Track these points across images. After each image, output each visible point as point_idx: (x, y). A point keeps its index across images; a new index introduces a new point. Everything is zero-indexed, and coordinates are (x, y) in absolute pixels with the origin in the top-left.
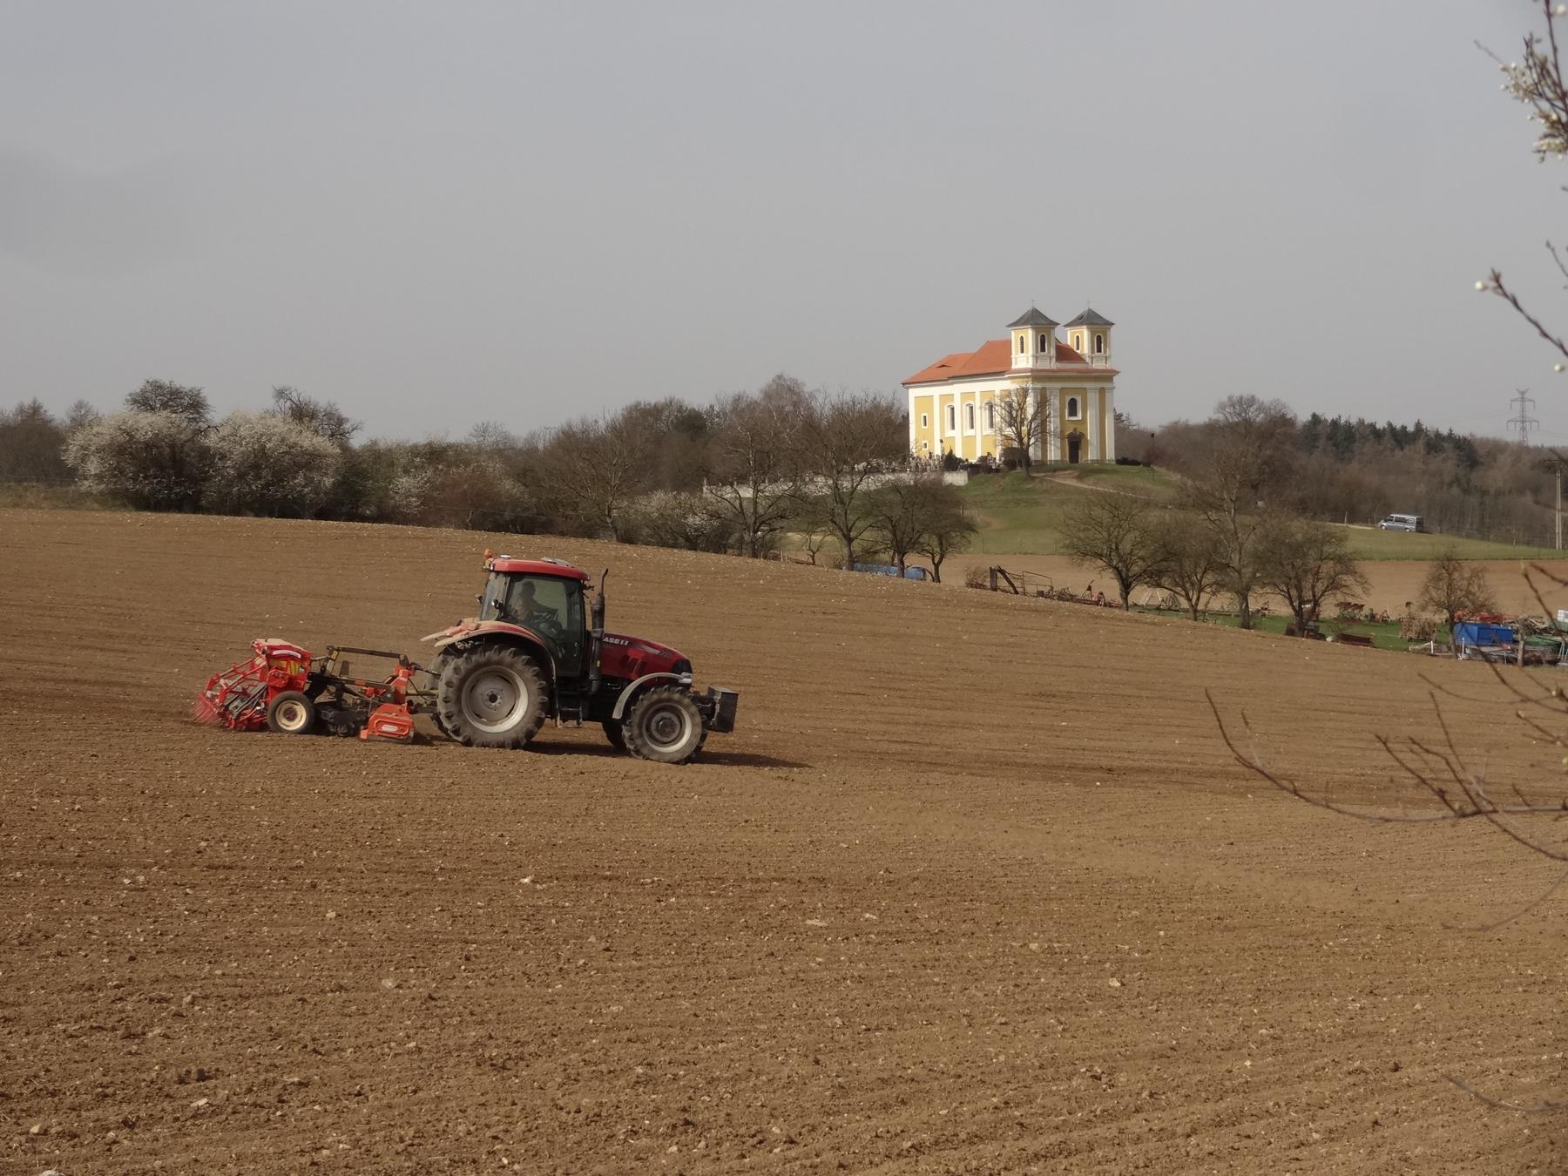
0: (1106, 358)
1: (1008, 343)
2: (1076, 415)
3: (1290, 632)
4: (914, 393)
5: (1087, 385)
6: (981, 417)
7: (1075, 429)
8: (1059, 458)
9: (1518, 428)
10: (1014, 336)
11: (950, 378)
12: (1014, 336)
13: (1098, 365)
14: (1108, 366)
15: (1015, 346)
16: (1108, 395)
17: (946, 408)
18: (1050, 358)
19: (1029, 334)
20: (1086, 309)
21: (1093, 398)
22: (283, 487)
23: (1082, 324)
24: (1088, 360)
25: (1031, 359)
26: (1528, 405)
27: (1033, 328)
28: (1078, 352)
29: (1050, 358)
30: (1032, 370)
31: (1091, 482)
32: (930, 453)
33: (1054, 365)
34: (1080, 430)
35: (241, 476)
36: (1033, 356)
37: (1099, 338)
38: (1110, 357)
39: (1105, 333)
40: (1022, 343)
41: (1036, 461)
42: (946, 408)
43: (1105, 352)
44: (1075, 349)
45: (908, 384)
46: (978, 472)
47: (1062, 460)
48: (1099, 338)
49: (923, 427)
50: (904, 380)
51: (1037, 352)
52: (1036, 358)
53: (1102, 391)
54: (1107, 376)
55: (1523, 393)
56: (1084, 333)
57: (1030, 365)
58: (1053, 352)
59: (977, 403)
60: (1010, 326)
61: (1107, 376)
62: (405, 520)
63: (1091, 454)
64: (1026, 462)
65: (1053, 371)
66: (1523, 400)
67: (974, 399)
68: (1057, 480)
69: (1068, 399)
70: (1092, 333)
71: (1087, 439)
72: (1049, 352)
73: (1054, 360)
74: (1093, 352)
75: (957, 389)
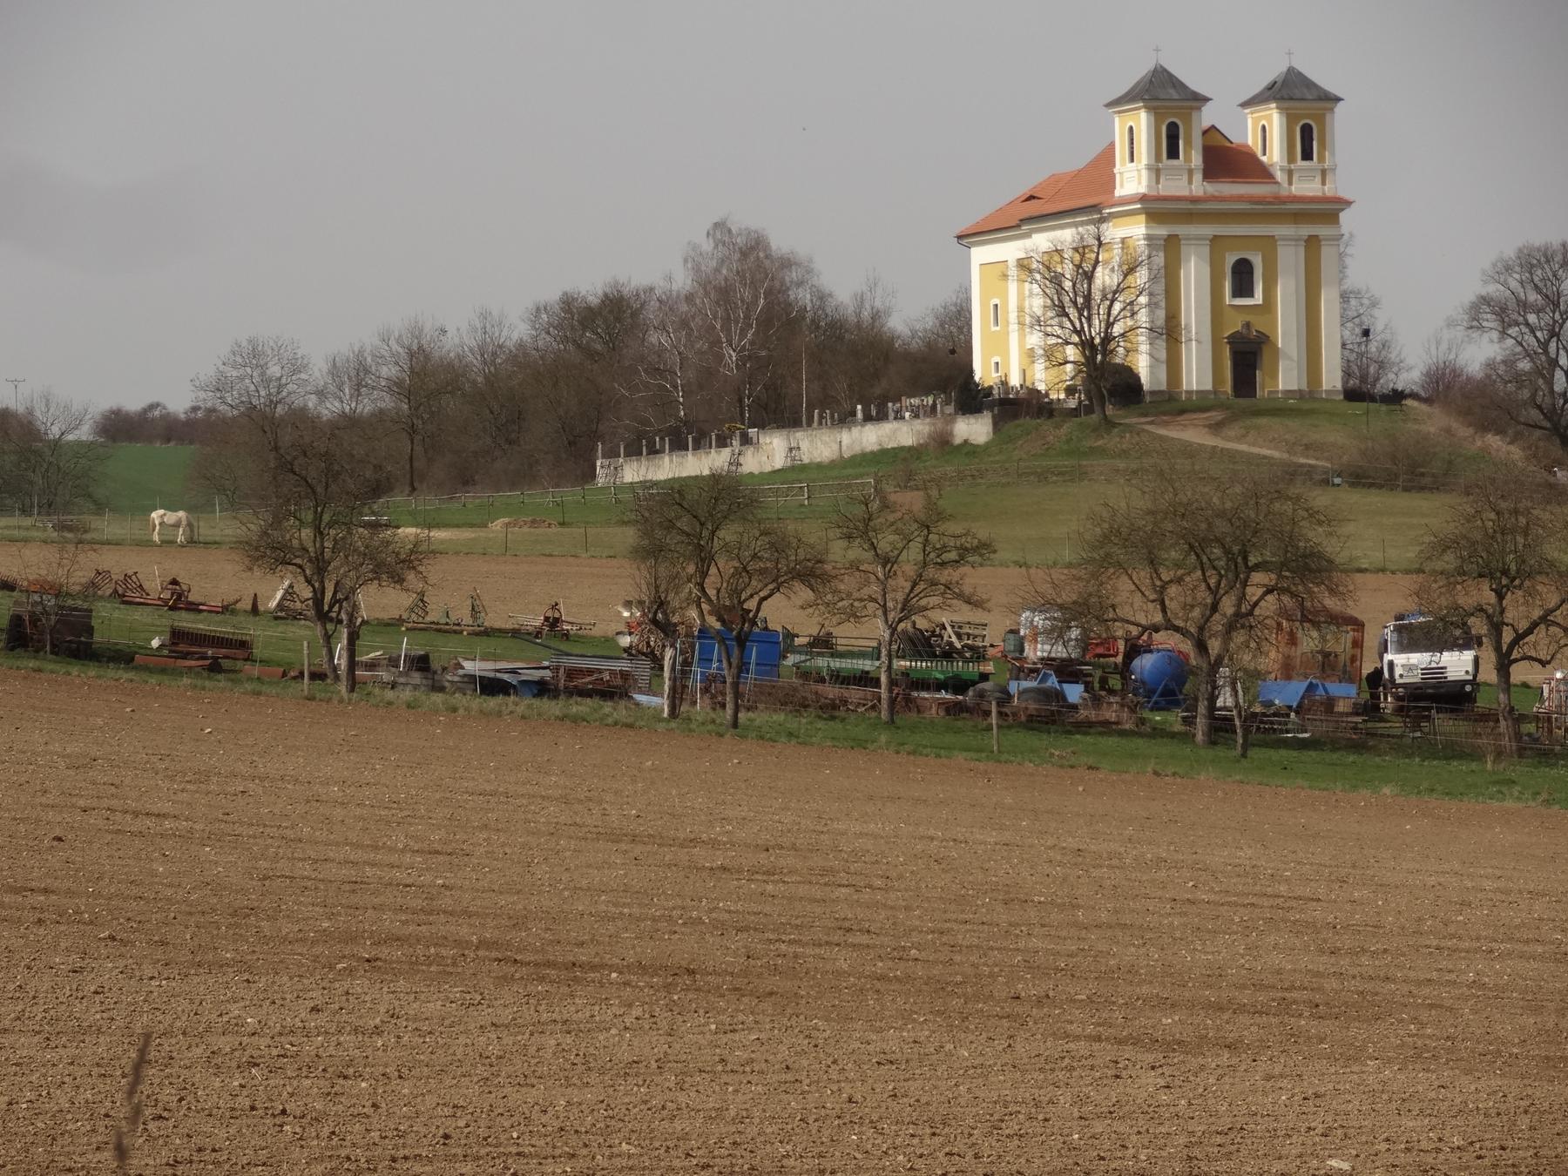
0: (1324, 173)
2: (1250, 294)
3: (172, 608)
4: (981, 255)
7: (1248, 325)
8: (1209, 386)
12: (1120, 125)
13: (1306, 186)
14: (1329, 190)
16: (1327, 253)
18: (1190, 172)
19: (1141, 120)
20: (1150, 66)
21: (1290, 259)
24: (1279, 176)
25: (1144, 173)
27: (1148, 109)
28: (1264, 159)
29: (1190, 172)
30: (1143, 199)
31: (1232, 433)
33: (1199, 187)
34: (1259, 324)
36: (1149, 168)
37: (1307, 132)
38: (1333, 170)
39: (1321, 120)
40: (1132, 148)
41: (1152, 393)
43: (1322, 159)
45: (967, 237)
46: (1016, 416)
47: (1215, 392)
50: (958, 232)
51: (1158, 158)
52: (1156, 172)
54: (1328, 211)
56: (1273, 118)
58: (1197, 159)
60: (1110, 105)
61: (1328, 211)
63: (1286, 377)
64: (1125, 388)
65: (1194, 200)
68: (1162, 432)
69: (1231, 259)
71: (1275, 346)
72: (1188, 159)
73: (1198, 177)
74: (1291, 159)
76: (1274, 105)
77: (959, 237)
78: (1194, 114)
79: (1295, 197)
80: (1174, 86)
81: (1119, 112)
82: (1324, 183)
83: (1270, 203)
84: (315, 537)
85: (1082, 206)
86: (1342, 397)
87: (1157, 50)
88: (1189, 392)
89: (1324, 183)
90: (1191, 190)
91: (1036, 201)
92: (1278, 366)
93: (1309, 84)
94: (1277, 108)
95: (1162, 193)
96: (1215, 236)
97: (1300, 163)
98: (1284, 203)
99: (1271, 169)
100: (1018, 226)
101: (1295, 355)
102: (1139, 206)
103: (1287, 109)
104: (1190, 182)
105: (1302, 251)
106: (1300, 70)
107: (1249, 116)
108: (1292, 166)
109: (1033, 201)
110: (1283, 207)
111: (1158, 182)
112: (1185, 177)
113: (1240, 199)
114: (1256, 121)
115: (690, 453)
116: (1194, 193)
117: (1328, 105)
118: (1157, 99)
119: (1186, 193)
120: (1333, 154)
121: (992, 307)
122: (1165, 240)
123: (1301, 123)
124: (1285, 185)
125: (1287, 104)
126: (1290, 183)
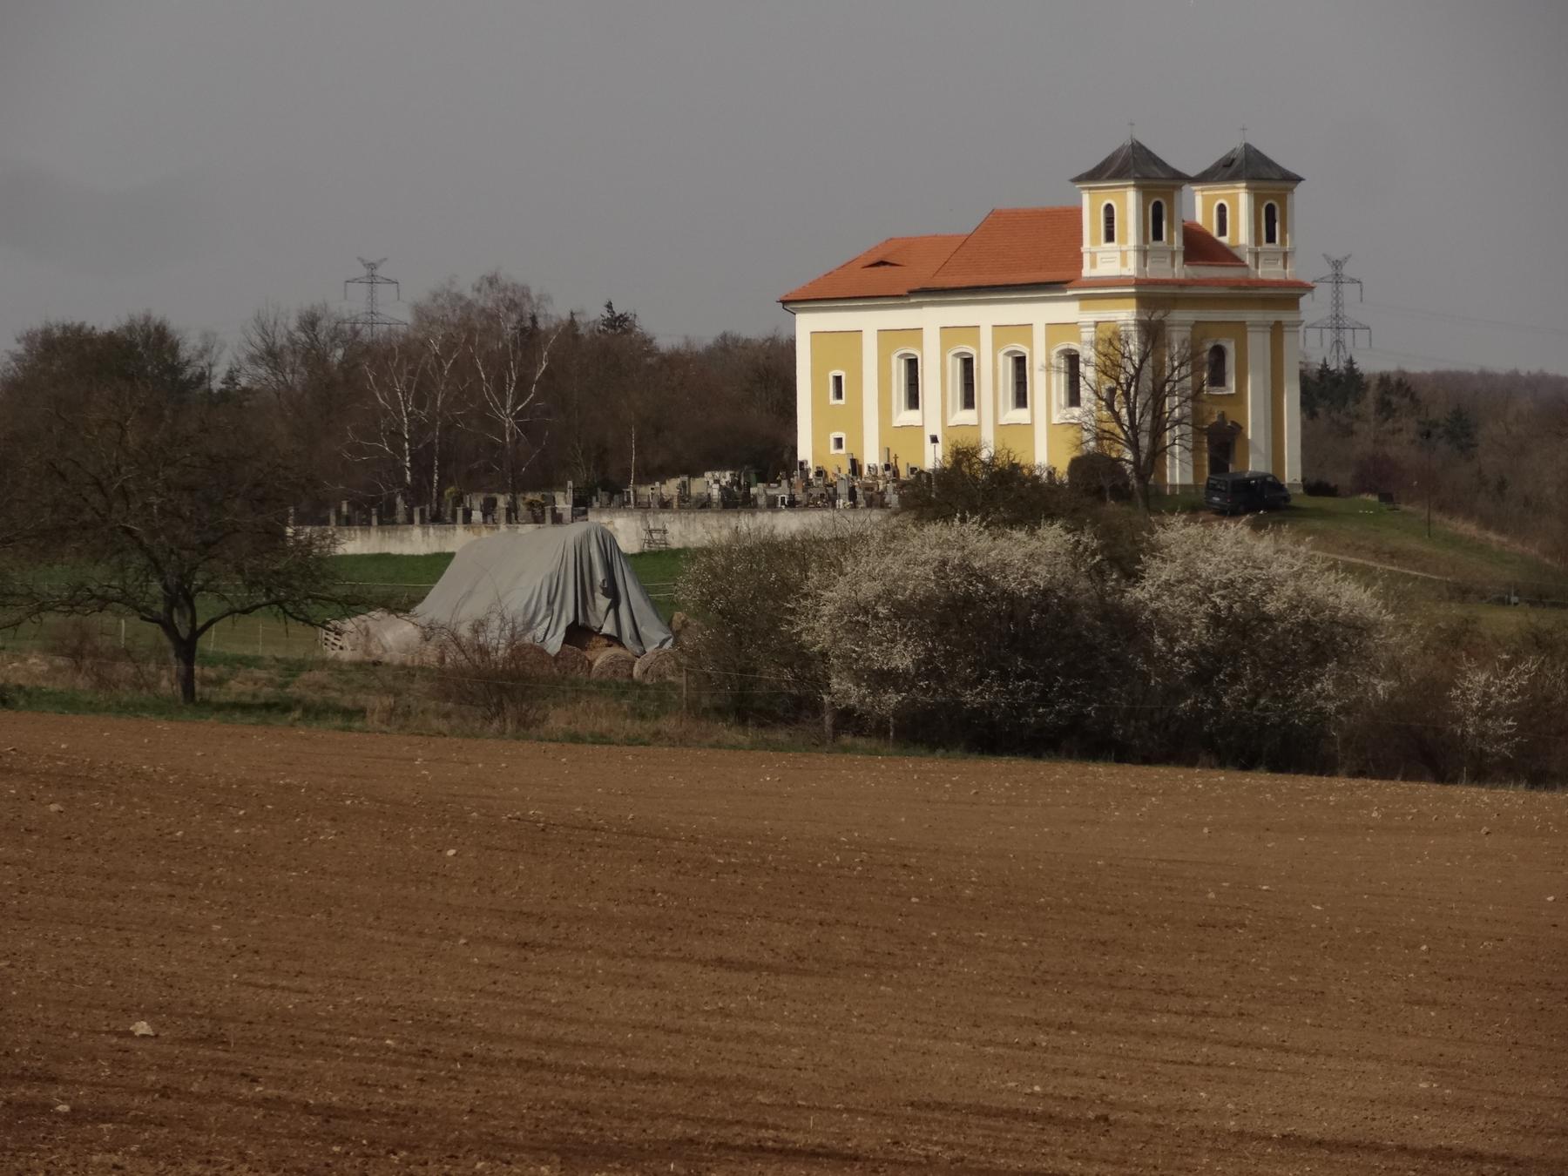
0: (1285, 254)
1: (1073, 217)
4: (807, 325)
5: (1251, 316)
6: (1046, 385)
7: (1222, 415)
8: (1190, 480)
9: (1327, 343)
10: (1090, 204)
11: (913, 293)
12: (1090, 204)
13: (1269, 271)
14: (1290, 273)
15: (1091, 224)
16: (1288, 338)
17: (894, 358)
18: (1173, 253)
19: (1128, 202)
21: (1258, 344)
22: (1287, 699)
23: (1234, 178)
24: (1248, 260)
25: (1132, 257)
26: (1349, 291)
27: (1138, 187)
28: (1225, 240)
29: (1173, 253)
30: (1138, 283)
32: (854, 462)
33: (1179, 270)
34: (1232, 416)
35: (1202, 678)
37: (1270, 210)
38: (1293, 252)
39: (1283, 199)
42: (894, 358)
44: (1214, 232)
45: (792, 303)
48: (1270, 210)
49: (833, 401)
50: (782, 295)
51: (1145, 241)
52: (1143, 253)
53: (1277, 330)
55: (1337, 264)
56: (1240, 200)
57: (1131, 269)
58: (1178, 242)
59: (1039, 357)
60: (1079, 179)
61: (1287, 296)
62: (1482, 773)
65: (1181, 284)
66: (1337, 280)
67: (977, 343)
70: (1257, 199)
71: (1245, 436)
72: (1170, 241)
73: (1179, 259)
74: (1258, 242)
75: (931, 319)
76: (1244, 185)
77: (785, 302)
78: (1176, 194)
79: (1263, 281)
80: (1156, 164)
81: (1090, 189)
82: (1285, 267)
83: (1245, 288)
84: (320, 604)
85: (1048, 280)
86: (1301, 491)
87: (1132, 124)
88: (1173, 486)
89: (1285, 267)
90: (1174, 274)
91: (887, 267)
92: (1248, 457)
93: (1270, 164)
94: (1246, 188)
95: (1149, 276)
96: (1197, 322)
97: (1265, 246)
98: (1257, 288)
99: (1236, 252)
100: (906, 297)
101: (1263, 450)
102: (1133, 290)
103: (1255, 189)
104: (1173, 265)
105: (1268, 336)
106: (1258, 148)
107: (1200, 193)
108: (1259, 249)
109: (882, 268)
110: (1247, 292)
111: (1145, 265)
112: (1168, 260)
113: (1219, 282)
114: (1206, 200)
115: (373, 531)
116: (1176, 277)
117: (1289, 185)
118: (1147, 178)
119: (1168, 276)
120: (1292, 237)
121: (831, 380)
122: (1193, 327)
123: (1266, 204)
124: (1253, 269)
125: (1255, 184)
126: (1257, 267)
